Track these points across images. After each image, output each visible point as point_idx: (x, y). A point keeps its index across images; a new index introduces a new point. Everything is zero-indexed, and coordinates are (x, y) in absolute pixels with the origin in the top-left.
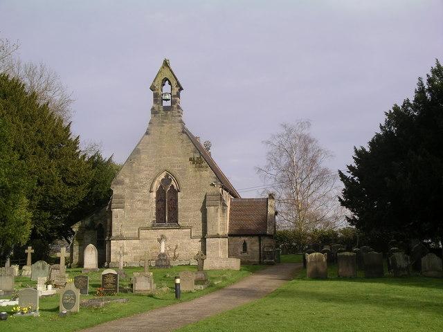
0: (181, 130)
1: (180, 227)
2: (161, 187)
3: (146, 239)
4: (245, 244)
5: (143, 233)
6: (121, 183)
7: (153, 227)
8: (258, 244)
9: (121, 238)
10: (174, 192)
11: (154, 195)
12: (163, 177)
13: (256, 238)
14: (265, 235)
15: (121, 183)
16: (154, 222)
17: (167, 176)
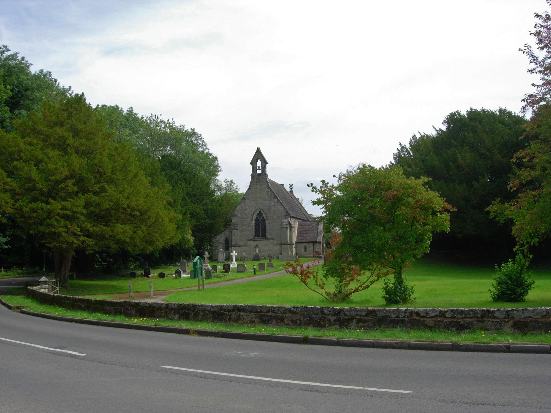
1: (268, 239)
2: (257, 218)
3: (251, 246)
5: (249, 243)
8: (312, 247)
11: (254, 222)
14: (316, 242)
15: (235, 216)
16: (254, 236)
17: (260, 212)
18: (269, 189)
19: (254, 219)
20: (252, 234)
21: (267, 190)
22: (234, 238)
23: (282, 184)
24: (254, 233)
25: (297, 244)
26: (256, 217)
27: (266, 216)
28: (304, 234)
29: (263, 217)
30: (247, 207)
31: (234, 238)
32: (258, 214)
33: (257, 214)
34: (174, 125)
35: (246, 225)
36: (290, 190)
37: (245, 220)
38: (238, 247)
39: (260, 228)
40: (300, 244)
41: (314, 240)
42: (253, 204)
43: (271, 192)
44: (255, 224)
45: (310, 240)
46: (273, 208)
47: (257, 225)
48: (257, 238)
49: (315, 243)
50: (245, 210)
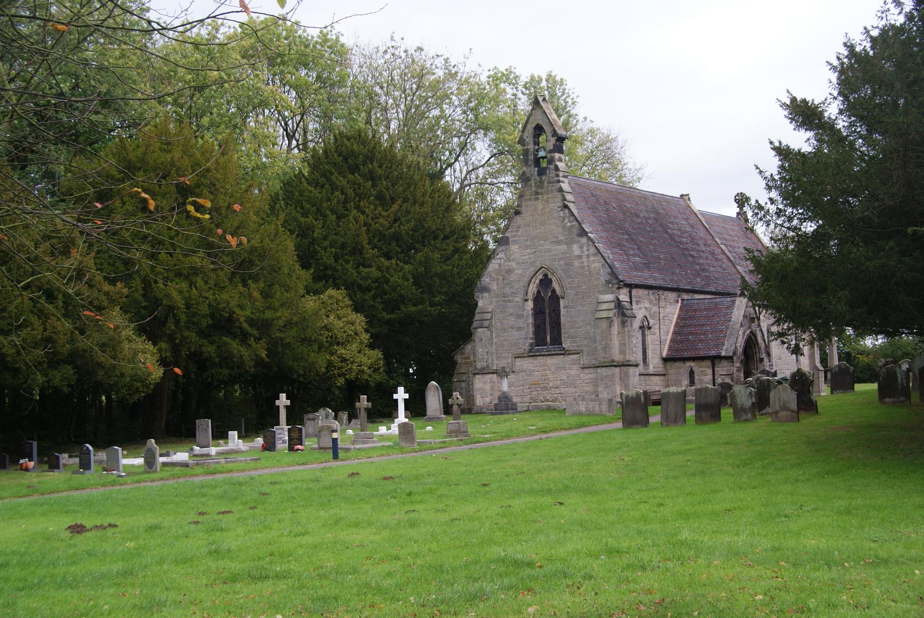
0: (560, 204)
1: (565, 353)
2: (539, 292)
3: (523, 371)
4: (692, 373)
5: (519, 363)
6: (486, 289)
7: (532, 353)
8: (710, 371)
9: (621, 371)
10: (555, 299)
11: (530, 305)
12: (541, 277)
13: (708, 363)
14: (719, 358)
15: (486, 289)
16: (531, 345)
17: (546, 275)
18: (567, 211)
19: (530, 296)
20: (526, 339)
21: (562, 214)
22: (480, 350)
23: (682, 196)
24: (531, 335)
25: (668, 364)
26: (535, 290)
27: (562, 287)
28: (691, 333)
29: (554, 291)
30: (514, 264)
31: (480, 350)
32: (541, 281)
33: (537, 281)
34: (451, 68)
35: (511, 315)
36: (738, 210)
37: (509, 301)
38: (490, 376)
39: (547, 322)
40: (679, 364)
41: (713, 353)
42: (528, 254)
43: (572, 219)
44: (534, 309)
45: (702, 353)
46: (576, 264)
47: (538, 312)
48: (538, 351)
49: (717, 361)
50: (509, 271)
